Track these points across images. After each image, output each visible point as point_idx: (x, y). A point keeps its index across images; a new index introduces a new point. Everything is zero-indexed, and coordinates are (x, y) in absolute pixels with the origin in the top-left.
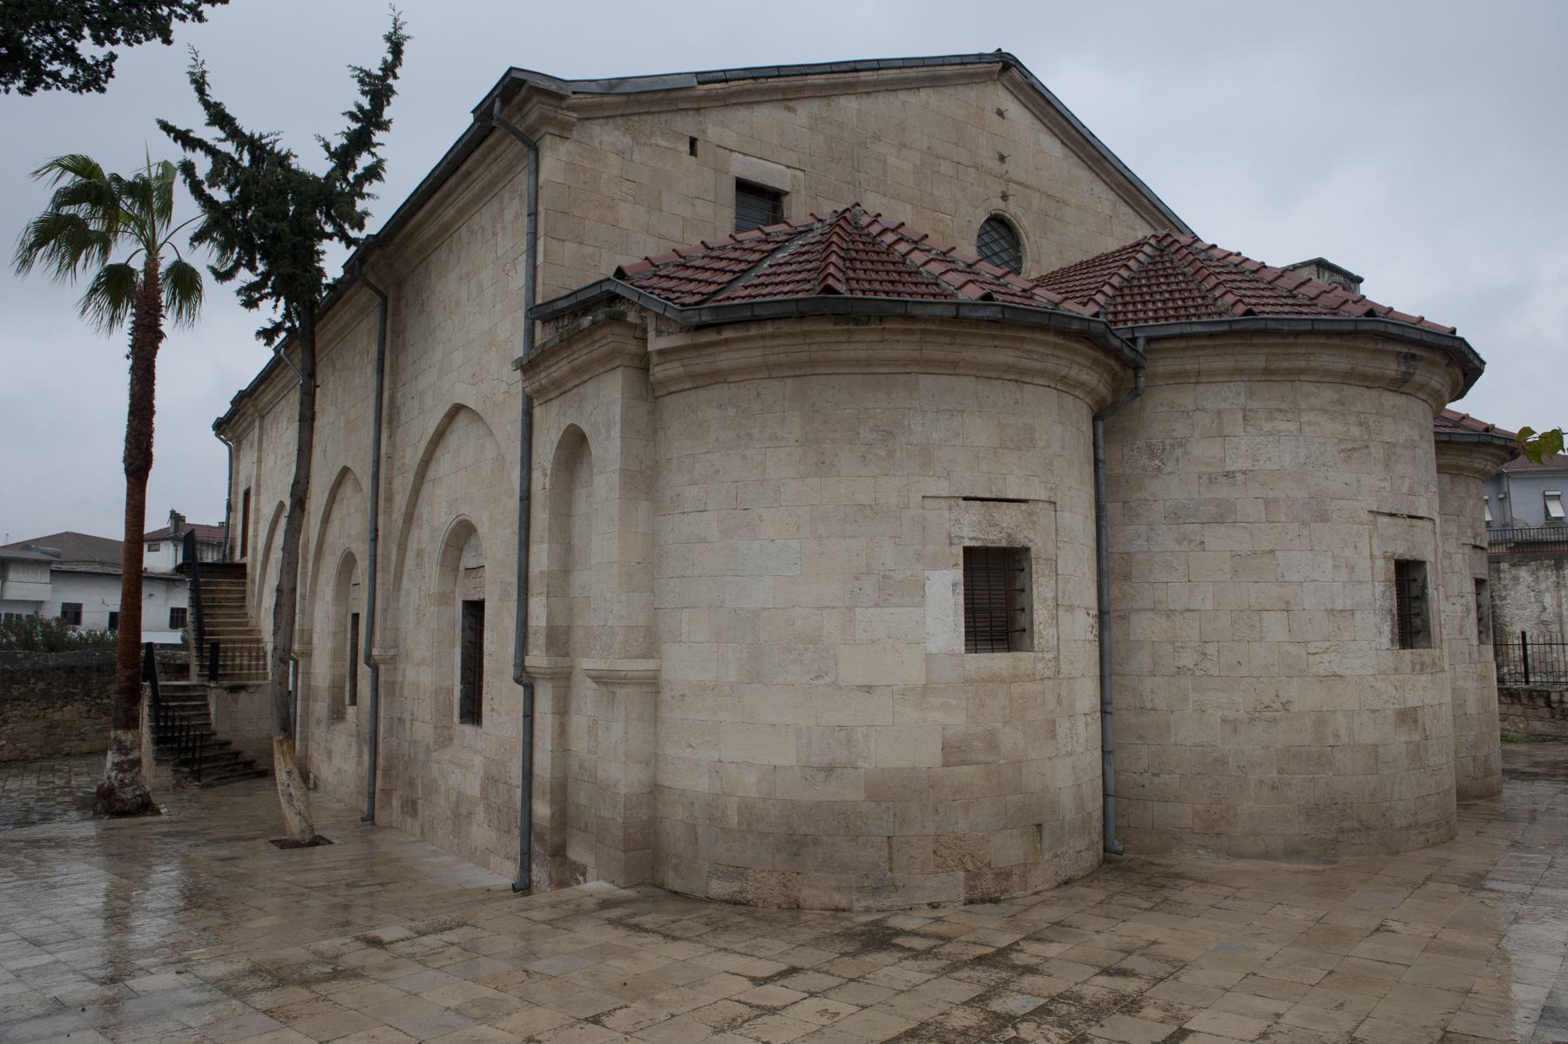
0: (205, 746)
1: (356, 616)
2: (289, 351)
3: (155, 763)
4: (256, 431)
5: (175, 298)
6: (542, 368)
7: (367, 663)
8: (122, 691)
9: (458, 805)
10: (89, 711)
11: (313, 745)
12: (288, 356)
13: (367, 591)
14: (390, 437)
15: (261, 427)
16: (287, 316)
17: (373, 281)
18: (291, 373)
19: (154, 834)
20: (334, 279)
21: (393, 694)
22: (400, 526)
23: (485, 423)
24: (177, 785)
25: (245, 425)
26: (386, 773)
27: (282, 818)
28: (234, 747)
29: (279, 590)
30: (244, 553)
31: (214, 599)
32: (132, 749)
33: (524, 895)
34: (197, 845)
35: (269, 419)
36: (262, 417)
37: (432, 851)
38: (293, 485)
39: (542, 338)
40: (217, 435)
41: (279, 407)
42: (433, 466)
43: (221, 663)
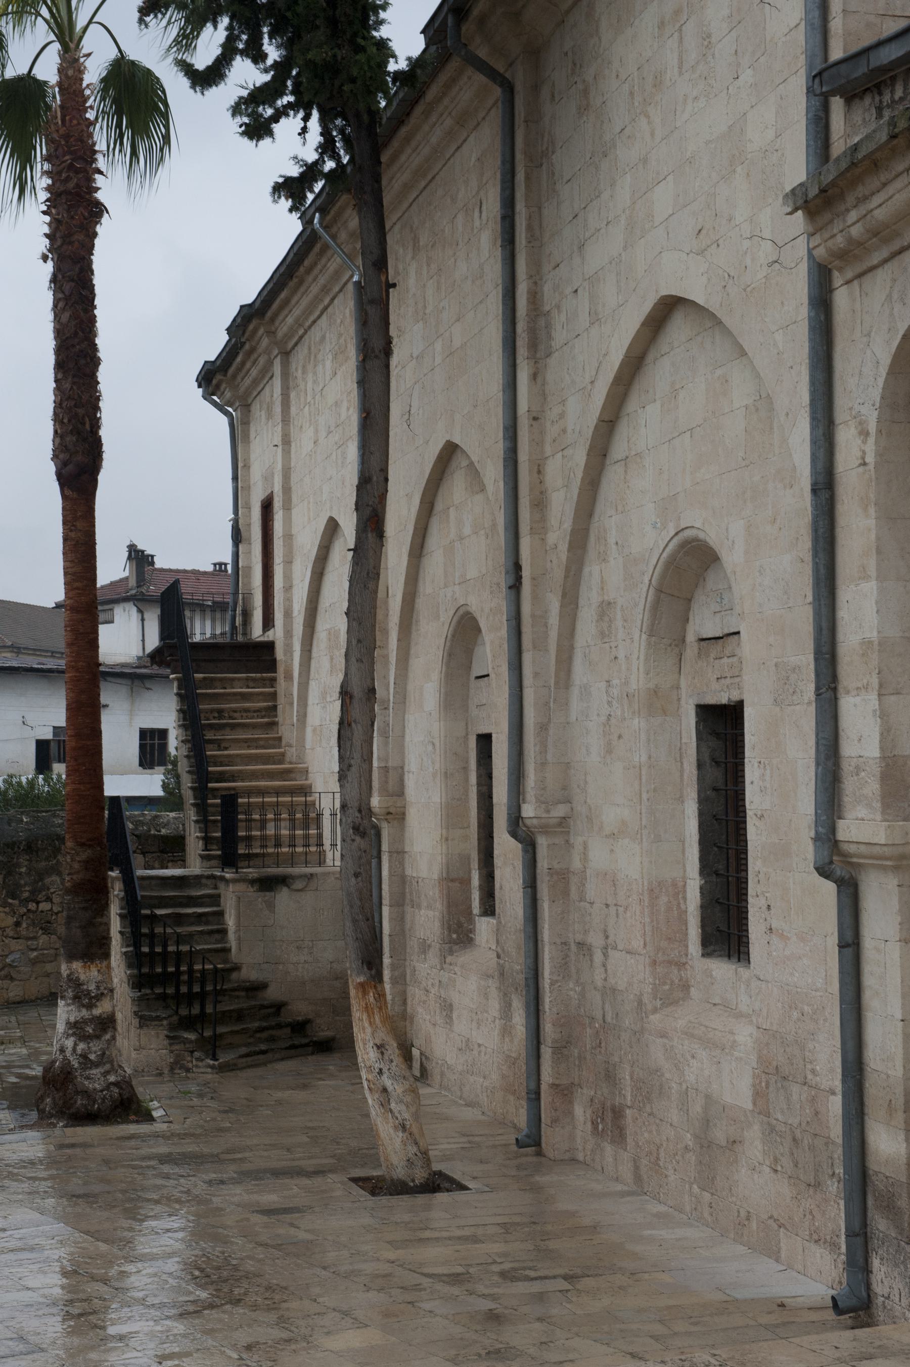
0: (223, 992)
1: (485, 740)
2: (329, 218)
3: (136, 1022)
4: (277, 383)
5: (121, 136)
6: (850, 199)
7: (514, 834)
8: (76, 889)
9: (707, 1122)
10: (18, 924)
11: (415, 994)
12: (326, 228)
13: (506, 688)
14: (534, 376)
15: (286, 375)
16: (327, 147)
17: (482, 53)
18: (334, 263)
19: (144, 1158)
20: (409, 59)
21: (566, 893)
22: (564, 557)
23: (727, 332)
24: (177, 1065)
25: (254, 372)
26: (560, 1050)
27: (371, 1132)
28: (273, 994)
29: (345, 694)
30: (268, 622)
31: (220, 712)
32: (100, 997)
33: (858, 1325)
34: (222, 1182)
35: (299, 356)
36: (286, 354)
37: (658, 1215)
38: (359, 488)
39: (847, 136)
40: (207, 396)
41: (315, 334)
42: (623, 430)
43: (241, 834)
